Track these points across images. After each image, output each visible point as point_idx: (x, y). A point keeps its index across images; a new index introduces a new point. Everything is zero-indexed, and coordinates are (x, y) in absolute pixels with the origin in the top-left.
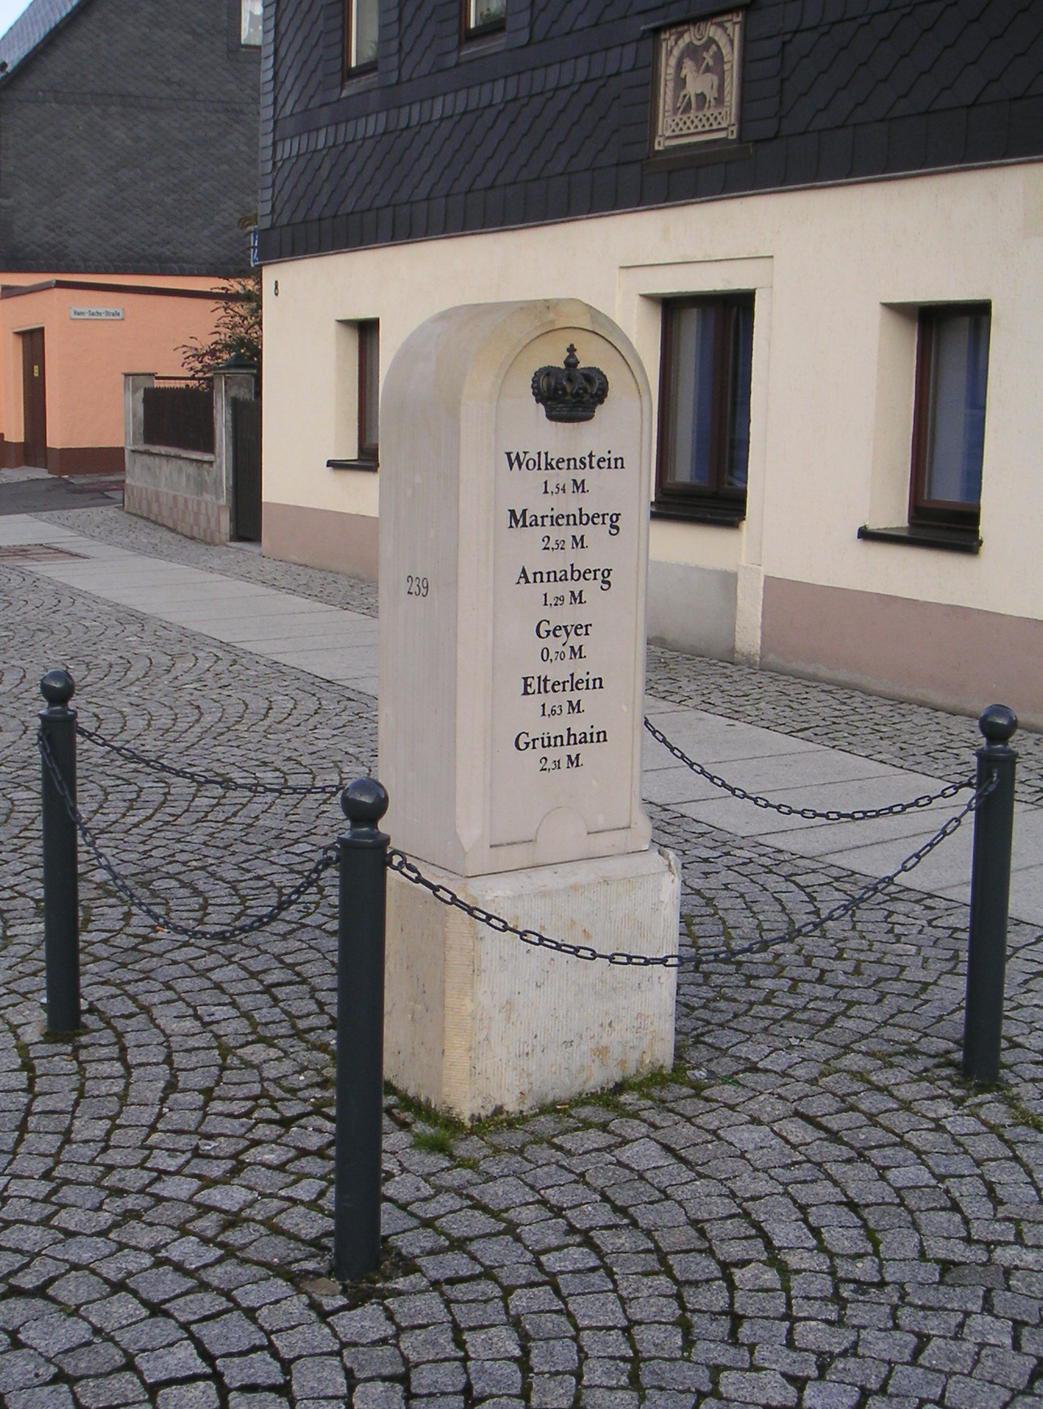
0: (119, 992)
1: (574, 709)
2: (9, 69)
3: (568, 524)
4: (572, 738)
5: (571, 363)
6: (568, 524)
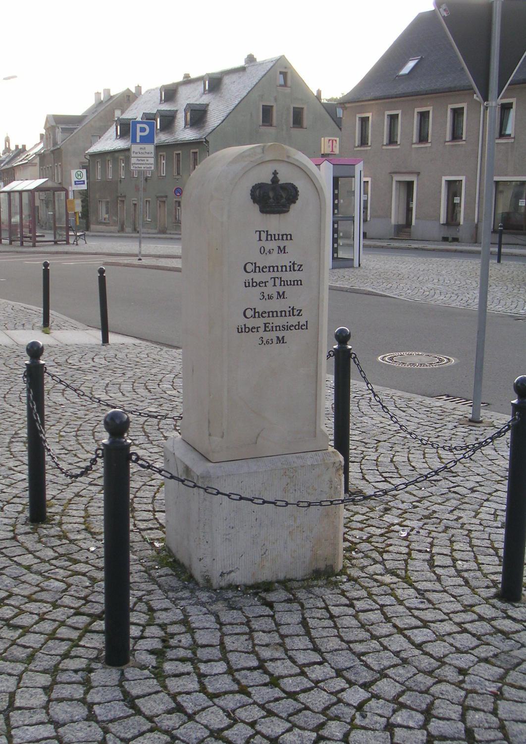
0: (447, 618)
1: (280, 297)
2: (189, 79)
3: (269, 271)
4: (282, 282)
5: (275, 180)
6: (269, 271)
